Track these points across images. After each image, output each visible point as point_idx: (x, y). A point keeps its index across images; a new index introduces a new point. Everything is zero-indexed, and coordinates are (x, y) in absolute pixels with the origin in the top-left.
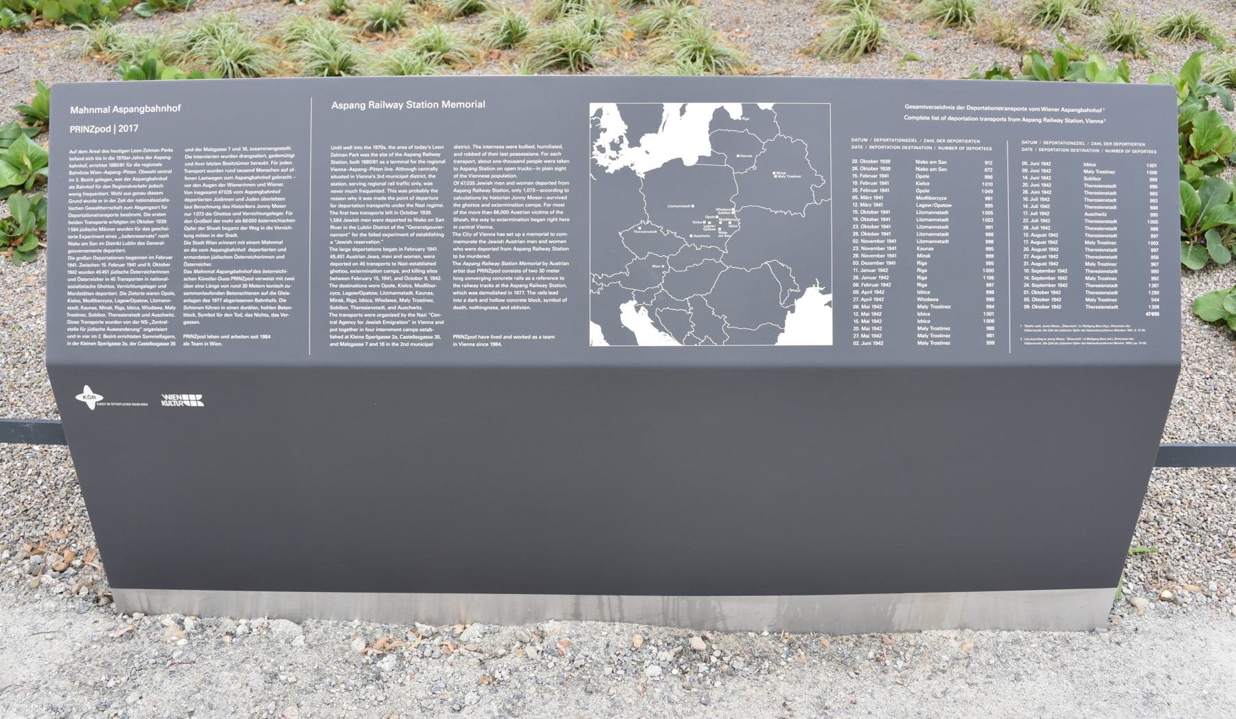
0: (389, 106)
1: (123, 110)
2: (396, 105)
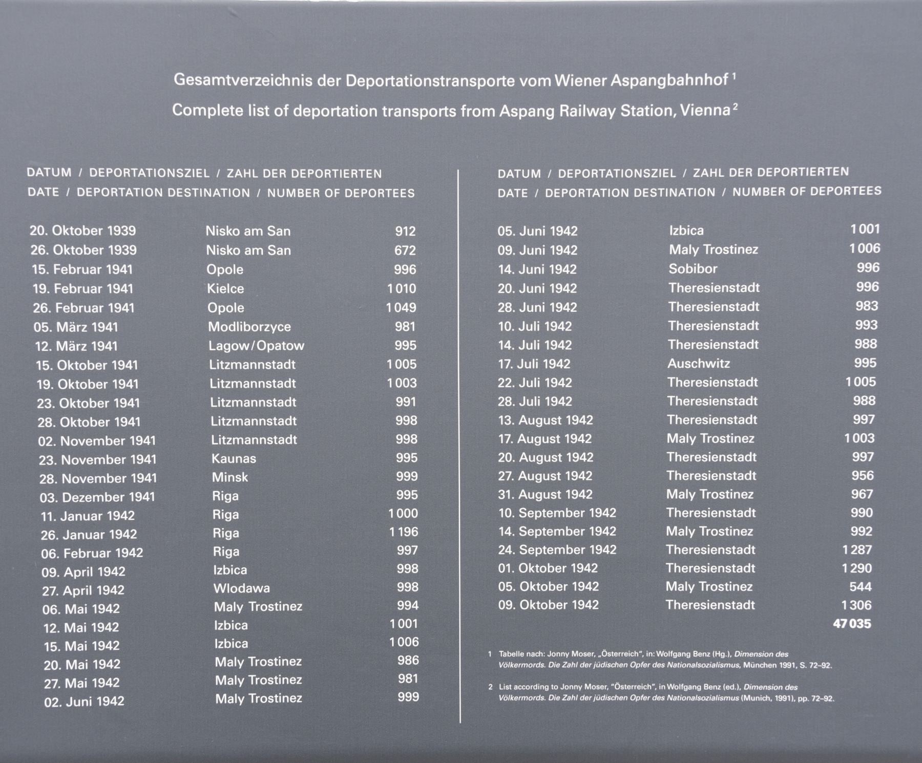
0: (593, 112)
1: (629, 82)
2: (604, 112)
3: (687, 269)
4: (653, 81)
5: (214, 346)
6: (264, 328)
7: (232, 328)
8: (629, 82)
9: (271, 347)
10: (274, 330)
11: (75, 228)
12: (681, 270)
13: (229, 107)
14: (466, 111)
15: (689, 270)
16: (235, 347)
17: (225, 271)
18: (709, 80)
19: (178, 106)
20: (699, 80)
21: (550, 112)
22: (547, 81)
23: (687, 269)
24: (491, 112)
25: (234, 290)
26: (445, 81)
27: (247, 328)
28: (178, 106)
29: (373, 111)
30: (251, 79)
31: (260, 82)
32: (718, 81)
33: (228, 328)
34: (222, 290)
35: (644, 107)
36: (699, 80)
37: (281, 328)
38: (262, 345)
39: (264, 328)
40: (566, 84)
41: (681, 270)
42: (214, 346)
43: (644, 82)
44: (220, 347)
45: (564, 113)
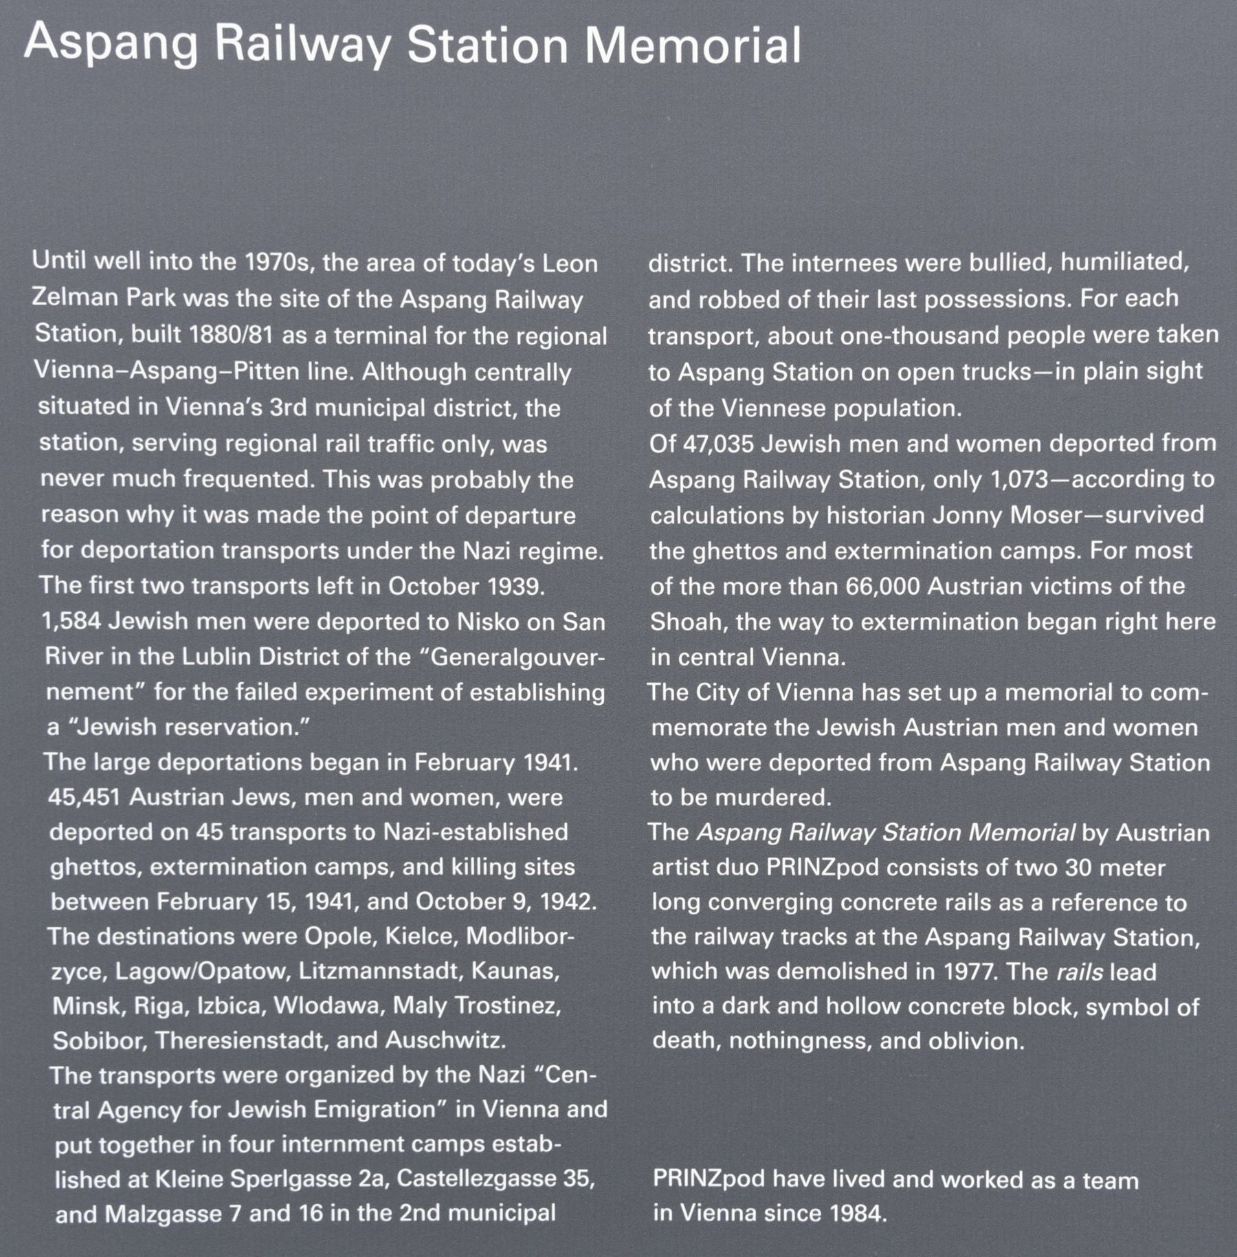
0: (320, 48)
3: (86, 1042)
5: (125, 972)
7: (510, 938)
9: (224, 973)
10: (69, 978)
11: (456, 896)
12: (76, 1043)
14: (1169, 443)
15: (91, 1043)
16: (164, 973)
17: (338, 938)
19: (405, 1173)
21: (775, 834)
23: (86, 1042)
24: (1210, 443)
25: (434, 938)
27: (537, 938)
28: (405, 1173)
33: (502, 938)
35: (73, 436)
37: (83, 973)
38: (207, 970)
40: (291, 1011)
41: (76, 1043)
42: (125, 972)
45: (229, 49)
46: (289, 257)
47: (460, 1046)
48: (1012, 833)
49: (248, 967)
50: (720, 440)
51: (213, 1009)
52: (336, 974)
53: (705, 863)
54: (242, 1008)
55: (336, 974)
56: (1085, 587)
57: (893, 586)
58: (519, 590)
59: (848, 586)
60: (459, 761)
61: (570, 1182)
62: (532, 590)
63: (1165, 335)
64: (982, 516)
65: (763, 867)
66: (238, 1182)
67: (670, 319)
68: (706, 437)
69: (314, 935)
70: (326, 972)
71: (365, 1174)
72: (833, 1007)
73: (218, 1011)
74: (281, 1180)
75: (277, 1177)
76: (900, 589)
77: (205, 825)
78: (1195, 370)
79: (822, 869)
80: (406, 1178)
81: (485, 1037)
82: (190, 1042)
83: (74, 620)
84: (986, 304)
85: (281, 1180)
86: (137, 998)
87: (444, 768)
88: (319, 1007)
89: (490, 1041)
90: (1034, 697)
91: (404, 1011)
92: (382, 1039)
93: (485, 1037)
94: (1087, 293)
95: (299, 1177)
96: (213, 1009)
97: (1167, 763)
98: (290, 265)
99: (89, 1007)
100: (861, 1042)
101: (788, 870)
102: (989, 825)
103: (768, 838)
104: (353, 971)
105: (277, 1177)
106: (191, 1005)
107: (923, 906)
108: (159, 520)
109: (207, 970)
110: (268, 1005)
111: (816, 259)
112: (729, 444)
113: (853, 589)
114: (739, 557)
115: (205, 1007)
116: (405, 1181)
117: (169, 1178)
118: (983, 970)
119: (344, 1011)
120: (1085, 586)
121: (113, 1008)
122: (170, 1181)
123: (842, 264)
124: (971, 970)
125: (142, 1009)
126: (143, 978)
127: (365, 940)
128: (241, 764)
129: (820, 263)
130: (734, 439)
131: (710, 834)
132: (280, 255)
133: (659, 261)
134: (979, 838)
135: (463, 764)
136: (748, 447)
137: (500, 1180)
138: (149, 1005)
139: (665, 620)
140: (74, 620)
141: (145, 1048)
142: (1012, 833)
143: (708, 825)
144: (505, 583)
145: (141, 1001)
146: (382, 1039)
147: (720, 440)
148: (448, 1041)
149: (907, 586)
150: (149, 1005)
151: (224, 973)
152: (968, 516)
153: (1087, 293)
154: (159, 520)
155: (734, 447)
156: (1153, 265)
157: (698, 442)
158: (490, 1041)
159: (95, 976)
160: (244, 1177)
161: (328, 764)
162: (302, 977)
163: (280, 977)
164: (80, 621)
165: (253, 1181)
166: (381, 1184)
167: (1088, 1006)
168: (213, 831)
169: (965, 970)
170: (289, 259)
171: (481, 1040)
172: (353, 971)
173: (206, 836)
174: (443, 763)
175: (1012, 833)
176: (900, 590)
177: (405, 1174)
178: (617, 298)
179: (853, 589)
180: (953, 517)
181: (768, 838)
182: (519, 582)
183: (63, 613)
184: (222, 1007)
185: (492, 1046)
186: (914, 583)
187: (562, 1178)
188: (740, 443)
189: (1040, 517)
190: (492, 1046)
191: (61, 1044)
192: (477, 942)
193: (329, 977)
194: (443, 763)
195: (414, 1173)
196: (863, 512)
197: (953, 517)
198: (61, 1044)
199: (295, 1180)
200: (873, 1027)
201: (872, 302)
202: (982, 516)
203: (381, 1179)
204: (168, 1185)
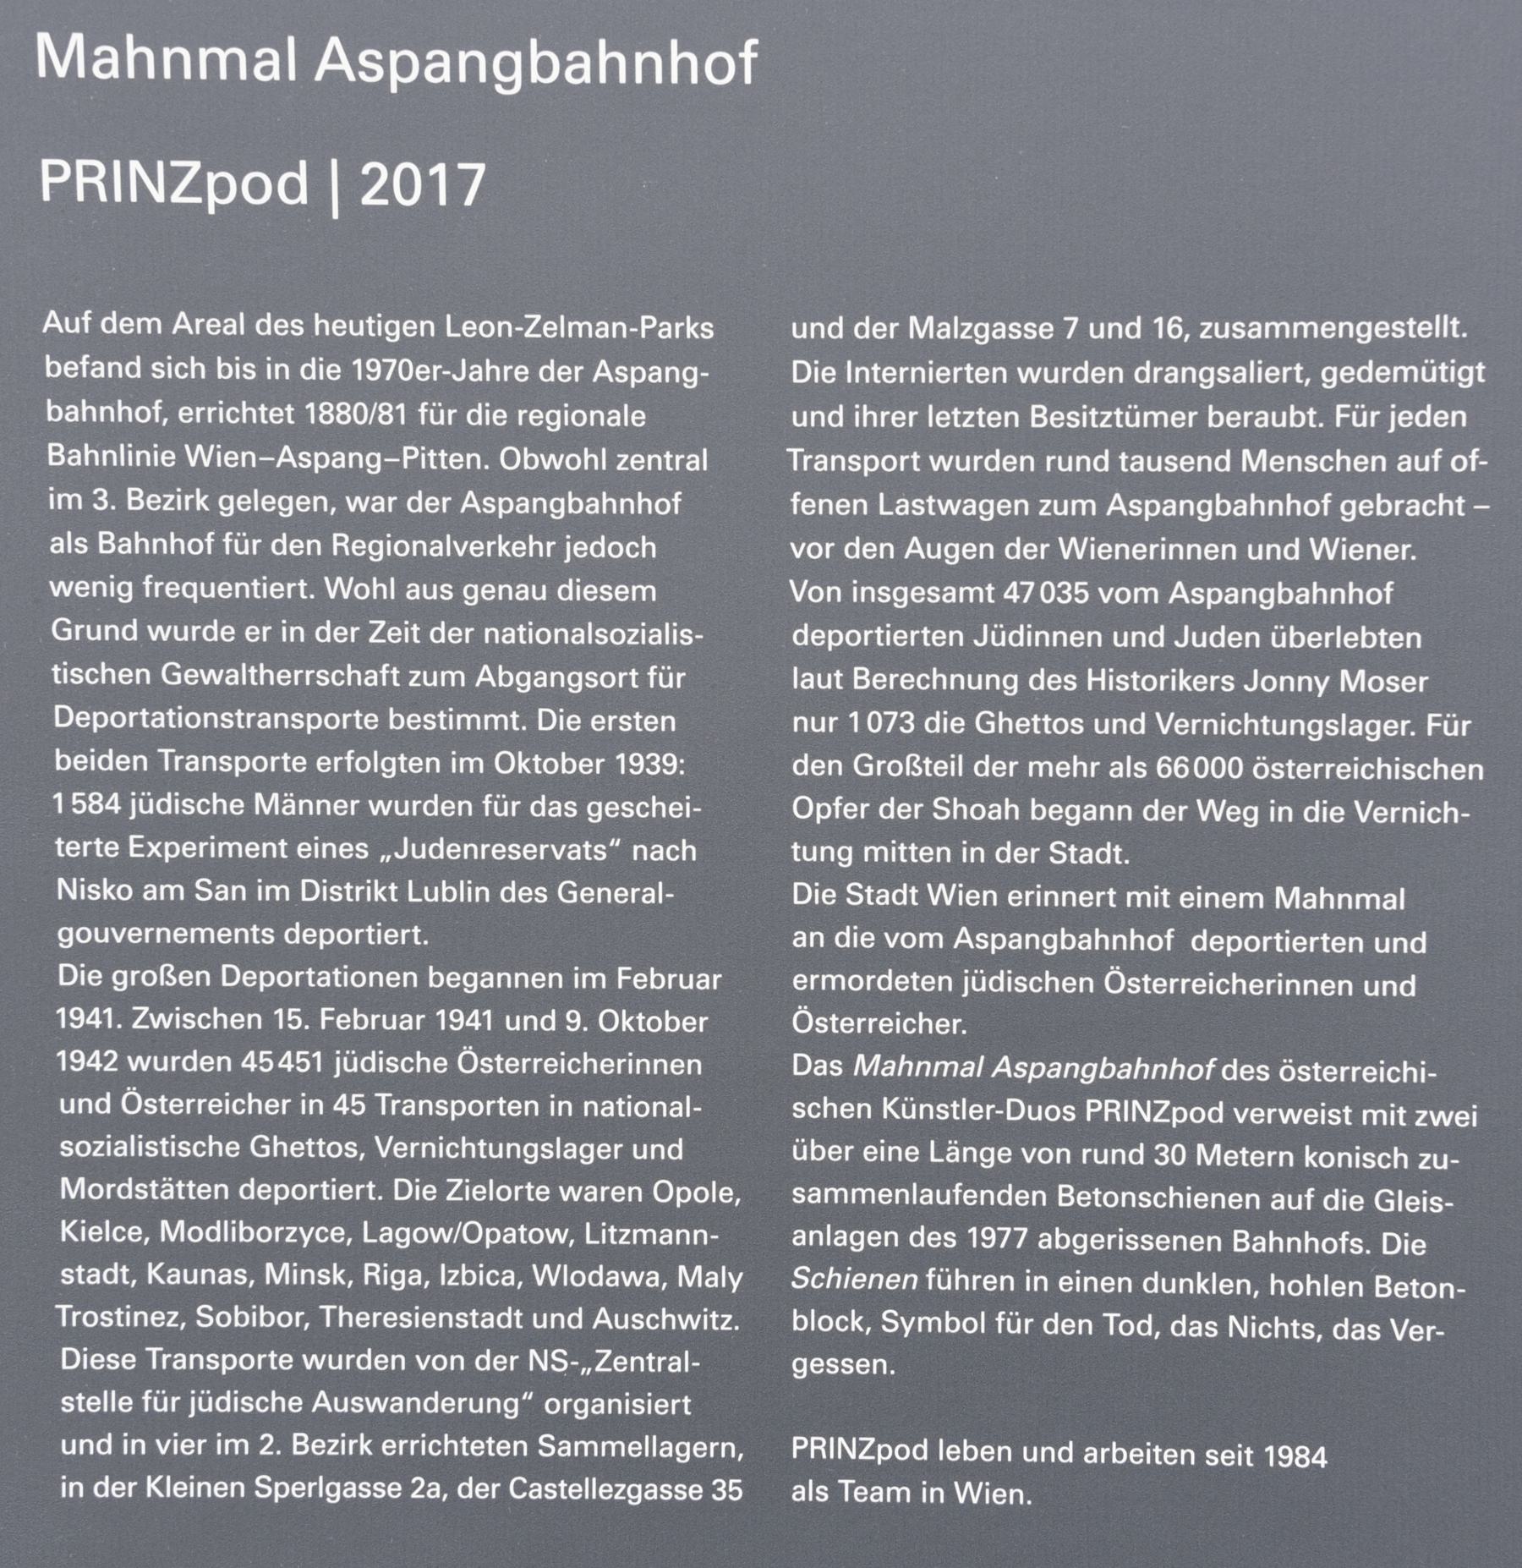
1: (384, 69)
4: (472, 63)
5: (374, 1233)
6: (284, 1234)
8: (384, 69)
9: (493, 1235)
10: (306, 1240)
13: (1408, 1281)
14: (152, 588)
15: (242, 1319)
16: (420, 1235)
17: (693, 1195)
18: (684, 65)
20: (649, 65)
22: (282, 891)
25: (120, 1234)
26: (244, 719)
29: (457, 1361)
30: (634, 891)
31: (627, 464)
32: (720, 68)
33: (204, 1234)
34: (92, 1234)
36: (649, 65)
37: (323, 1235)
38: (472, 1232)
39: (284, 1234)
42: (374, 1233)
43: (441, 67)
44: (388, 1235)
46: (406, 365)
47: (684, 1327)
48: (942, 1067)
49: (522, 1229)
50: (1048, 588)
51: (458, 1279)
52: (630, 1237)
53: (1347, 1110)
54: (493, 1278)
55: (630, 1237)
56: (467, 764)
57: (1210, 768)
58: (653, 769)
59: (1159, 767)
60: (671, 977)
61: (719, 1494)
62: (670, 769)
63: (1128, 462)
64: (1305, 683)
65: (1081, 1111)
66: (264, 1491)
67: (817, 440)
68: (1032, 584)
69: (663, 1191)
70: (618, 1236)
71: (418, 1483)
72: (1278, 1287)
73: (464, 1282)
74: (315, 1489)
75: (311, 1485)
76: (1218, 771)
77: (288, 1054)
78: (1456, 505)
79: (1153, 1114)
80: (520, 1488)
81: (714, 1316)
82: (361, 1320)
83: (88, 803)
84: (1057, 423)
85: (315, 1489)
86: (367, 1265)
87: (653, 986)
88: (586, 1279)
89: (720, 1321)
90: (1086, 902)
91: (690, 1284)
92: (589, 1317)
93: (714, 1316)
94: (1343, 411)
95: (338, 1485)
96: (458, 1279)
97: (332, 977)
98: (406, 374)
99: (308, 1276)
100: (1309, 1332)
101: (1112, 1115)
102: (877, 1057)
103: (1080, 1076)
104: (649, 1235)
105: (311, 1485)
106: (431, 1274)
107: (1248, 1160)
108: (1310, 689)
109: (472, 1232)
110: (525, 1275)
111: (876, 368)
112: (1059, 592)
113: (1164, 771)
114: (1036, 731)
115: (448, 1276)
116: (518, 1492)
117: (162, 1486)
118: (1015, 1236)
119: (617, 1284)
120: (467, 763)
121: (338, 1277)
122: (163, 1490)
123: (907, 374)
124: (1000, 1235)
125: (372, 1279)
126: (849, 1244)
127: (726, 1198)
128: (325, 979)
129: (880, 373)
130: (1065, 587)
131: (1008, 1070)
132: (394, 361)
133: (313, 367)
134: (865, 1073)
135: (676, 981)
136: (1081, 596)
137: (634, 1491)
138: (381, 1274)
139: (950, 806)
140: (88, 803)
141: (307, 1325)
142: (942, 1067)
143: (1006, 1058)
144: (636, 760)
145: (372, 1269)
146: (589, 1317)
147: (1048, 588)
148: (669, 1321)
149: (1227, 768)
150: (381, 1274)
151: (493, 1235)
152: (1287, 682)
153: (1343, 411)
154: (1310, 689)
155: (1065, 597)
156: (880, 377)
157: (1022, 590)
158: (720, 1321)
159: (338, 1238)
160: (272, 1485)
161: (451, 979)
162: (588, 1241)
163: (562, 1241)
164: (93, 804)
165: (282, 1490)
166: (438, 1495)
167: (63, 1273)
168: (262, 1060)
169: (993, 1237)
170: (406, 366)
171: (710, 1320)
172: (649, 1235)
173: (253, 1066)
174: (651, 980)
175: (942, 1067)
176: (1218, 772)
177: (518, 1483)
178: (741, 412)
179: (1164, 771)
180: (1269, 684)
181: (1080, 1076)
182: (653, 759)
183: (75, 795)
184: (469, 1278)
185: (723, 1327)
186: (1236, 763)
187: (710, 1490)
188: (1072, 592)
189: (1376, 684)
190: (723, 1327)
191: (205, 1321)
192: (73, 1196)
193: (621, 1242)
194: (651, 980)
195: (530, 1482)
196: (1135, 676)
197: (1269, 684)
198: (205, 1321)
199: (333, 1490)
200: (1323, 1311)
201: (921, 419)
202: (1305, 683)
203: (438, 1489)
204: (161, 1495)
